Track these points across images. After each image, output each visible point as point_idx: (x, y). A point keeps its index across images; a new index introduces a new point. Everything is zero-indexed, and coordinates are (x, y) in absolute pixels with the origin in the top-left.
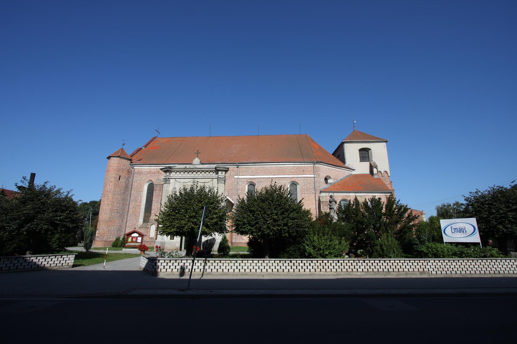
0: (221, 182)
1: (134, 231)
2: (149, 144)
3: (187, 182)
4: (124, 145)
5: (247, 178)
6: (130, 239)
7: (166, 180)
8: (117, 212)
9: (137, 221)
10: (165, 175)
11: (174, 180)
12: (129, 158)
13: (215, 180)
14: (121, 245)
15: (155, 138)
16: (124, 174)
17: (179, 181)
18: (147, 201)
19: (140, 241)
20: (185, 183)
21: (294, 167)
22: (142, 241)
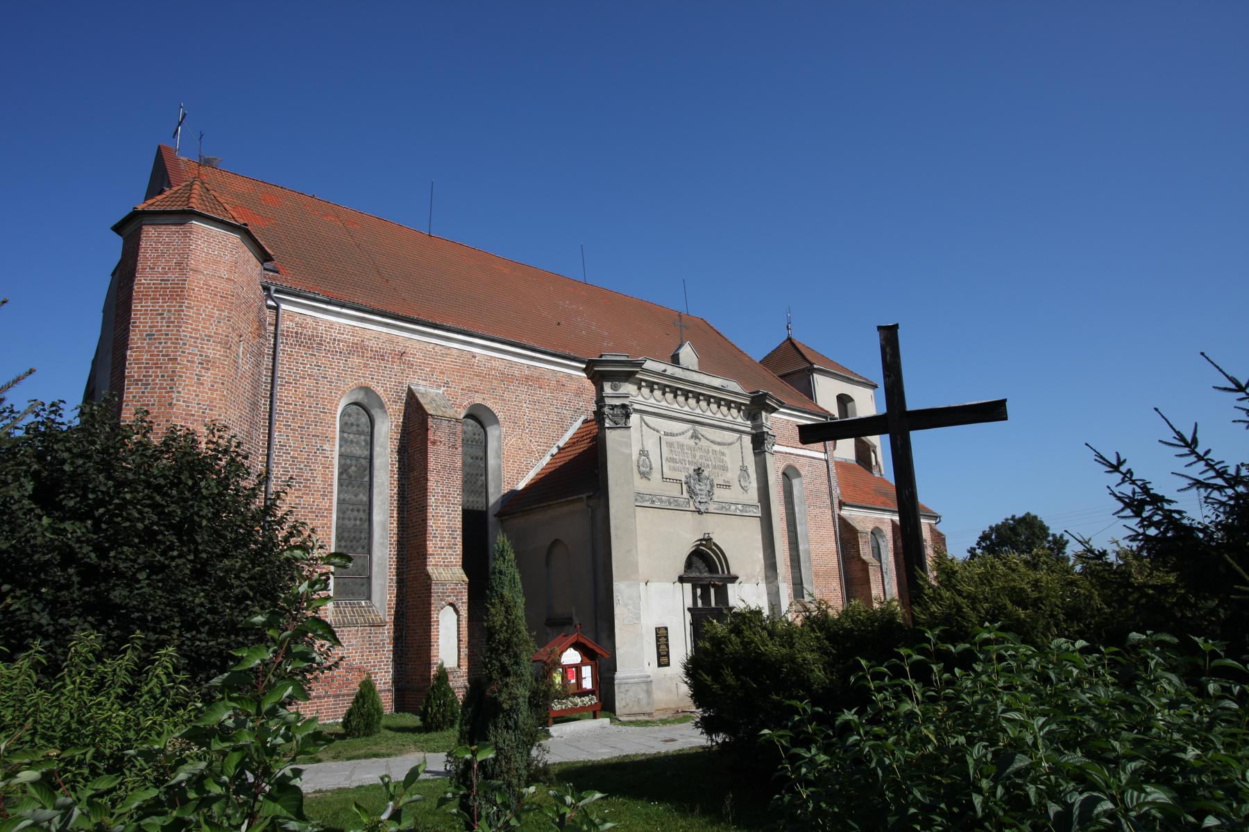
3: (677, 435)
18: (466, 482)
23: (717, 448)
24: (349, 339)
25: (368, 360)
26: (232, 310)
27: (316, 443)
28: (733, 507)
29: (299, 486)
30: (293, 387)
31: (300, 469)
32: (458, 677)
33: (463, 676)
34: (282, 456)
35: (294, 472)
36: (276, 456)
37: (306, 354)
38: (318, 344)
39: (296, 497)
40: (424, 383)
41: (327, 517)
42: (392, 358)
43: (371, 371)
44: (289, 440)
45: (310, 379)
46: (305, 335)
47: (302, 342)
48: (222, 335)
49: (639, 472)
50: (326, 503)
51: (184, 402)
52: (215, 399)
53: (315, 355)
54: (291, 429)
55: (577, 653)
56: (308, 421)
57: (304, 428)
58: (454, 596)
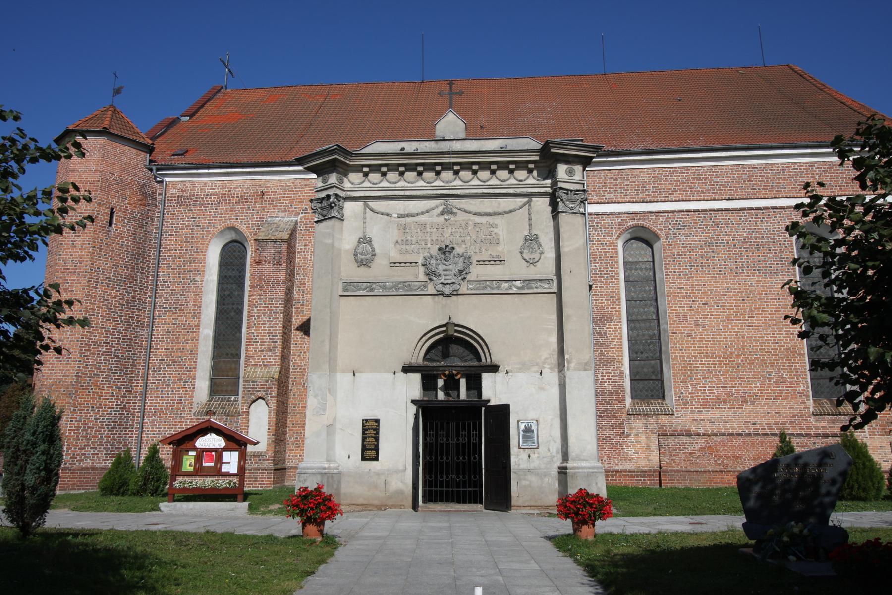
0: (572, 209)
1: (204, 426)
2: (202, 106)
3: (417, 214)
4: (118, 92)
5: (620, 213)
6: (189, 461)
7: (325, 203)
8: (108, 353)
9: (189, 385)
10: (320, 185)
11: (360, 204)
12: (142, 141)
13: (542, 205)
14: (145, 484)
15: (219, 91)
16: (125, 204)
17: (382, 210)
18: (221, 311)
19: (233, 468)
20: (408, 216)
21: (812, 164)
22: (242, 469)
23: (483, 220)
24: (219, 192)
25: (233, 205)
26: (97, 192)
27: (190, 276)
28: (505, 285)
29: (176, 310)
30: (174, 237)
31: (177, 297)
32: (264, 460)
33: (268, 460)
34: (164, 290)
35: (172, 300)
36: (160, 290)
37: (184, 211)
38: (194, 201)
39: (173, 319)
40: (283, 214)
41: (195, 332)
42: (255, 199)
43: (236, 213)
44: (170, 277)
45: (187, 229)
46: (185, 197)
47: (182, 202)
48: (90, 210)
49: (356, 261)
50: (196, 321)
51: (63, 261)
52: (84, 255)
53: (192, 210)
54: (172, 269)
55: (220, 438)
56: (184, 261)
57: (181, 266)
58: (264, 391)
